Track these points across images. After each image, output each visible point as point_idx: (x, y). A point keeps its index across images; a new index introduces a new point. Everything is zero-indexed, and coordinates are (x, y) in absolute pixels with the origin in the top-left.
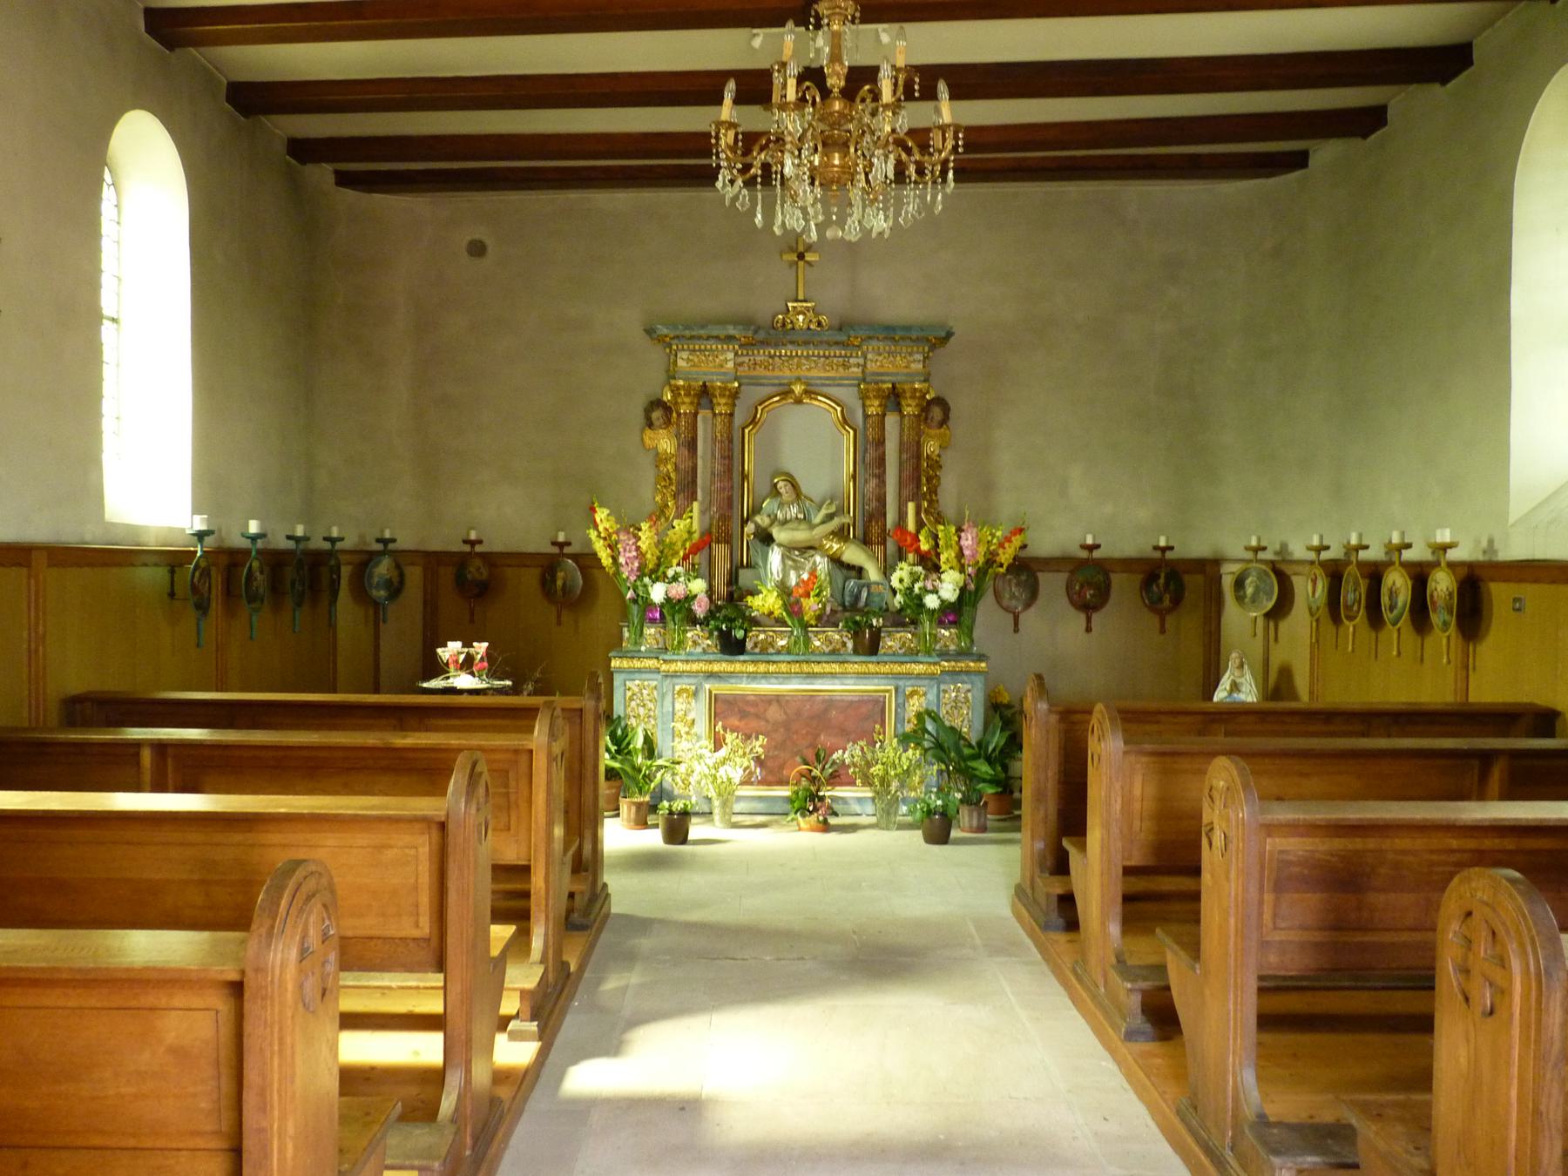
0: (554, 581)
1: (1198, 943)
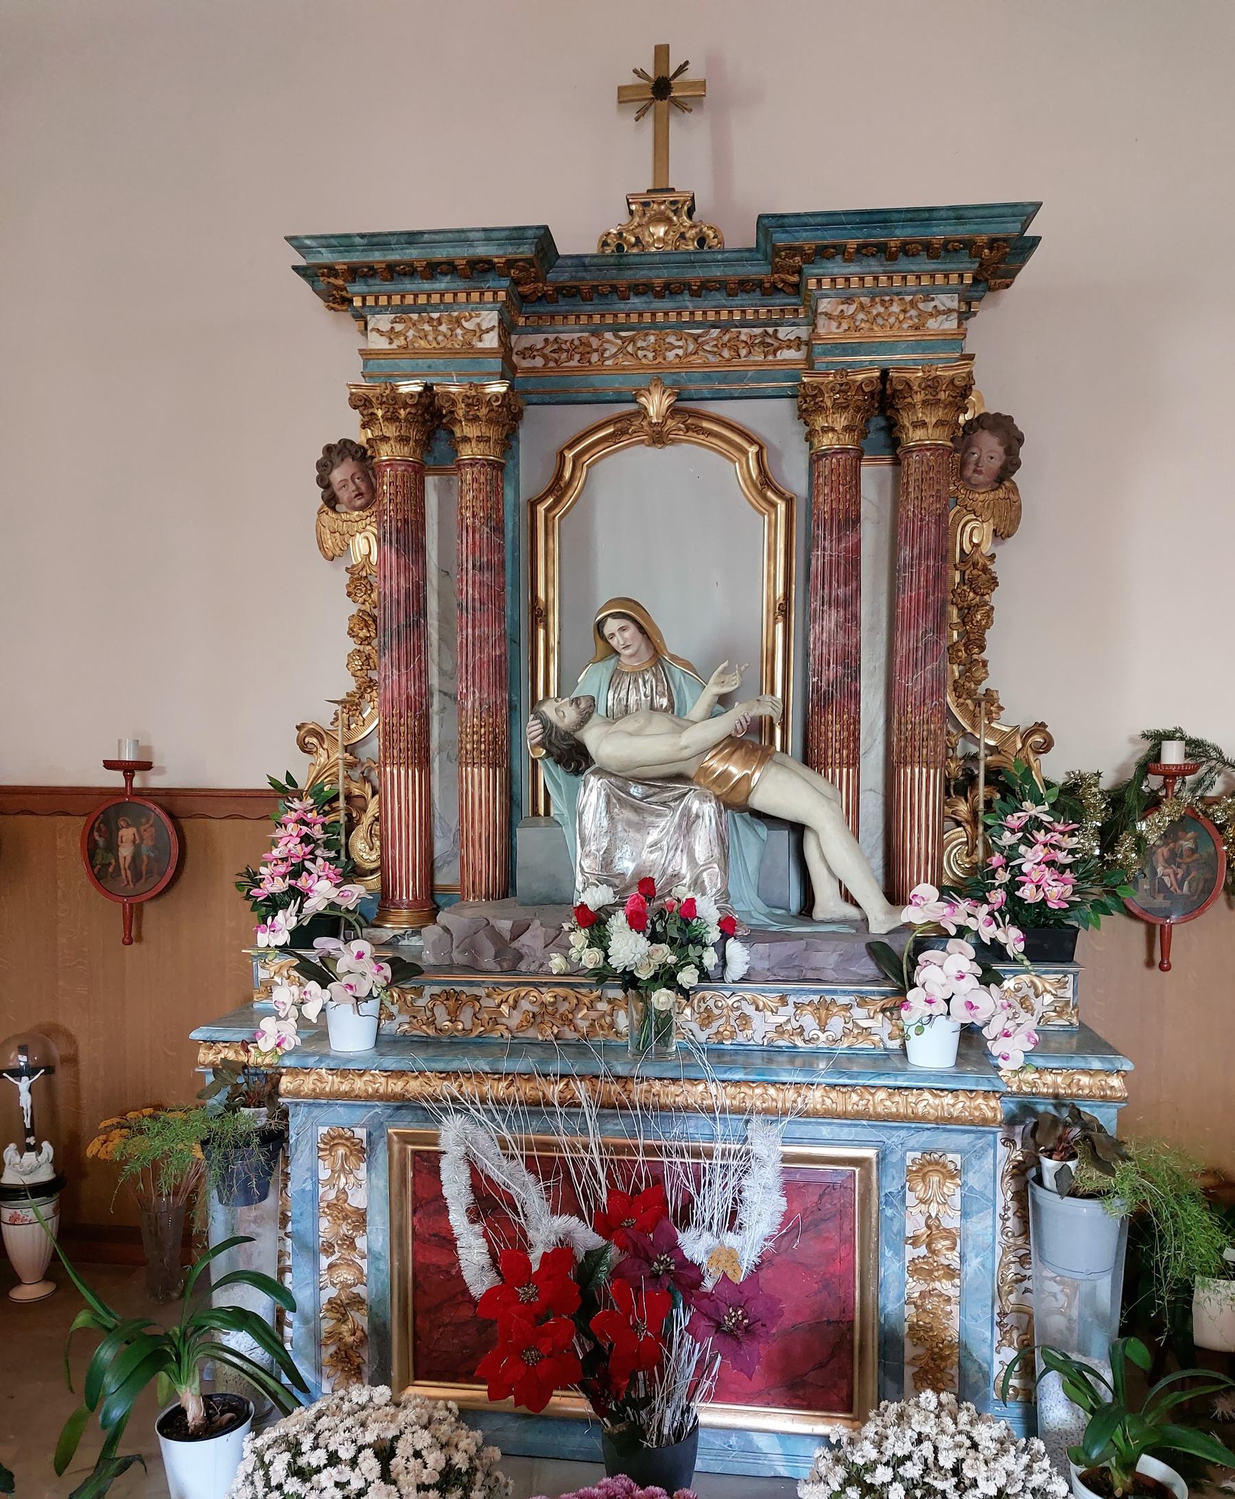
0: (112, 847)
1: (303, 276)
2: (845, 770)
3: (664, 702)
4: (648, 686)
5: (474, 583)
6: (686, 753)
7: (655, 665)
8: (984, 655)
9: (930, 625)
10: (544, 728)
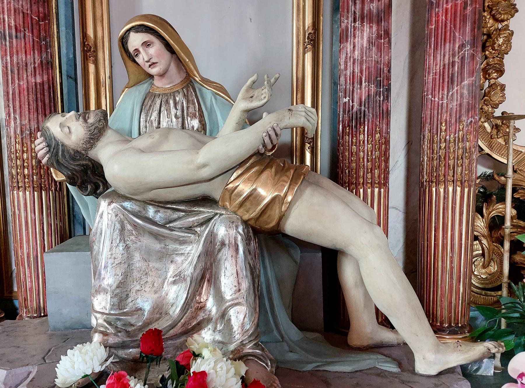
2: (376, 190)
3: (195, 123)
4: (179, 107)
5: (9, 10)
6: (205, 173)
7: (187, 87)
8: (501, 80)
9: (468, 38)
10: (49, 146)
